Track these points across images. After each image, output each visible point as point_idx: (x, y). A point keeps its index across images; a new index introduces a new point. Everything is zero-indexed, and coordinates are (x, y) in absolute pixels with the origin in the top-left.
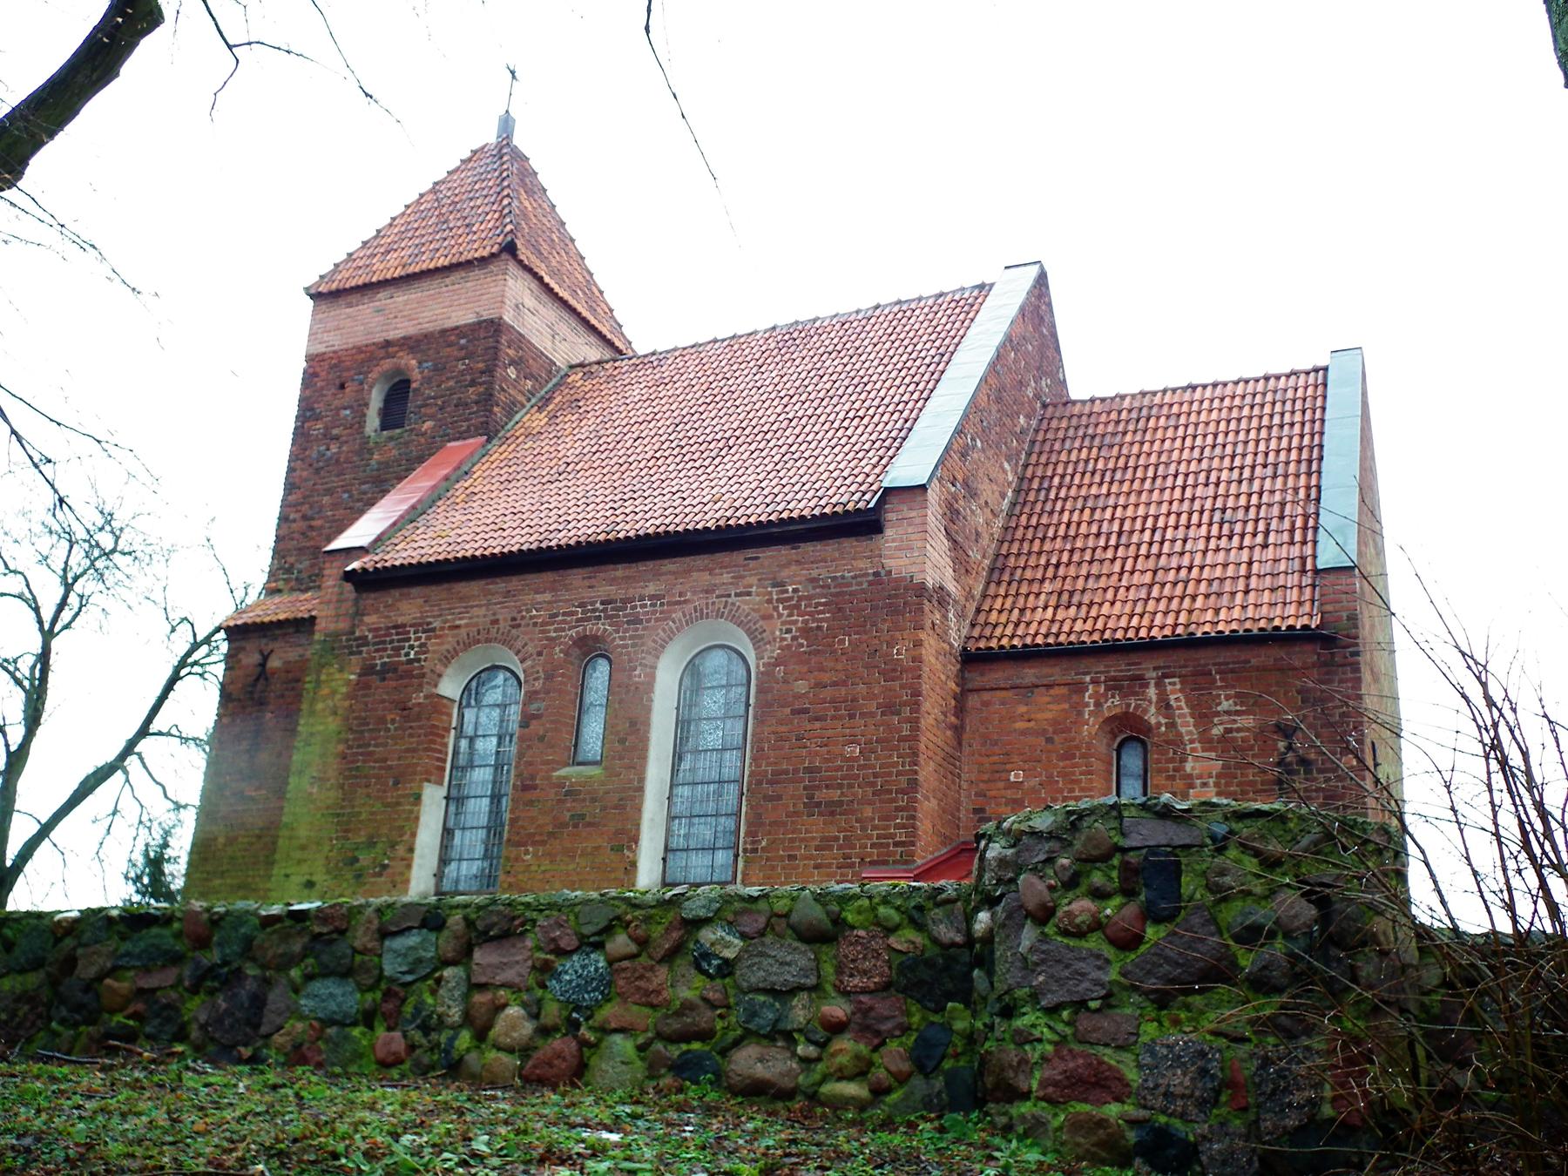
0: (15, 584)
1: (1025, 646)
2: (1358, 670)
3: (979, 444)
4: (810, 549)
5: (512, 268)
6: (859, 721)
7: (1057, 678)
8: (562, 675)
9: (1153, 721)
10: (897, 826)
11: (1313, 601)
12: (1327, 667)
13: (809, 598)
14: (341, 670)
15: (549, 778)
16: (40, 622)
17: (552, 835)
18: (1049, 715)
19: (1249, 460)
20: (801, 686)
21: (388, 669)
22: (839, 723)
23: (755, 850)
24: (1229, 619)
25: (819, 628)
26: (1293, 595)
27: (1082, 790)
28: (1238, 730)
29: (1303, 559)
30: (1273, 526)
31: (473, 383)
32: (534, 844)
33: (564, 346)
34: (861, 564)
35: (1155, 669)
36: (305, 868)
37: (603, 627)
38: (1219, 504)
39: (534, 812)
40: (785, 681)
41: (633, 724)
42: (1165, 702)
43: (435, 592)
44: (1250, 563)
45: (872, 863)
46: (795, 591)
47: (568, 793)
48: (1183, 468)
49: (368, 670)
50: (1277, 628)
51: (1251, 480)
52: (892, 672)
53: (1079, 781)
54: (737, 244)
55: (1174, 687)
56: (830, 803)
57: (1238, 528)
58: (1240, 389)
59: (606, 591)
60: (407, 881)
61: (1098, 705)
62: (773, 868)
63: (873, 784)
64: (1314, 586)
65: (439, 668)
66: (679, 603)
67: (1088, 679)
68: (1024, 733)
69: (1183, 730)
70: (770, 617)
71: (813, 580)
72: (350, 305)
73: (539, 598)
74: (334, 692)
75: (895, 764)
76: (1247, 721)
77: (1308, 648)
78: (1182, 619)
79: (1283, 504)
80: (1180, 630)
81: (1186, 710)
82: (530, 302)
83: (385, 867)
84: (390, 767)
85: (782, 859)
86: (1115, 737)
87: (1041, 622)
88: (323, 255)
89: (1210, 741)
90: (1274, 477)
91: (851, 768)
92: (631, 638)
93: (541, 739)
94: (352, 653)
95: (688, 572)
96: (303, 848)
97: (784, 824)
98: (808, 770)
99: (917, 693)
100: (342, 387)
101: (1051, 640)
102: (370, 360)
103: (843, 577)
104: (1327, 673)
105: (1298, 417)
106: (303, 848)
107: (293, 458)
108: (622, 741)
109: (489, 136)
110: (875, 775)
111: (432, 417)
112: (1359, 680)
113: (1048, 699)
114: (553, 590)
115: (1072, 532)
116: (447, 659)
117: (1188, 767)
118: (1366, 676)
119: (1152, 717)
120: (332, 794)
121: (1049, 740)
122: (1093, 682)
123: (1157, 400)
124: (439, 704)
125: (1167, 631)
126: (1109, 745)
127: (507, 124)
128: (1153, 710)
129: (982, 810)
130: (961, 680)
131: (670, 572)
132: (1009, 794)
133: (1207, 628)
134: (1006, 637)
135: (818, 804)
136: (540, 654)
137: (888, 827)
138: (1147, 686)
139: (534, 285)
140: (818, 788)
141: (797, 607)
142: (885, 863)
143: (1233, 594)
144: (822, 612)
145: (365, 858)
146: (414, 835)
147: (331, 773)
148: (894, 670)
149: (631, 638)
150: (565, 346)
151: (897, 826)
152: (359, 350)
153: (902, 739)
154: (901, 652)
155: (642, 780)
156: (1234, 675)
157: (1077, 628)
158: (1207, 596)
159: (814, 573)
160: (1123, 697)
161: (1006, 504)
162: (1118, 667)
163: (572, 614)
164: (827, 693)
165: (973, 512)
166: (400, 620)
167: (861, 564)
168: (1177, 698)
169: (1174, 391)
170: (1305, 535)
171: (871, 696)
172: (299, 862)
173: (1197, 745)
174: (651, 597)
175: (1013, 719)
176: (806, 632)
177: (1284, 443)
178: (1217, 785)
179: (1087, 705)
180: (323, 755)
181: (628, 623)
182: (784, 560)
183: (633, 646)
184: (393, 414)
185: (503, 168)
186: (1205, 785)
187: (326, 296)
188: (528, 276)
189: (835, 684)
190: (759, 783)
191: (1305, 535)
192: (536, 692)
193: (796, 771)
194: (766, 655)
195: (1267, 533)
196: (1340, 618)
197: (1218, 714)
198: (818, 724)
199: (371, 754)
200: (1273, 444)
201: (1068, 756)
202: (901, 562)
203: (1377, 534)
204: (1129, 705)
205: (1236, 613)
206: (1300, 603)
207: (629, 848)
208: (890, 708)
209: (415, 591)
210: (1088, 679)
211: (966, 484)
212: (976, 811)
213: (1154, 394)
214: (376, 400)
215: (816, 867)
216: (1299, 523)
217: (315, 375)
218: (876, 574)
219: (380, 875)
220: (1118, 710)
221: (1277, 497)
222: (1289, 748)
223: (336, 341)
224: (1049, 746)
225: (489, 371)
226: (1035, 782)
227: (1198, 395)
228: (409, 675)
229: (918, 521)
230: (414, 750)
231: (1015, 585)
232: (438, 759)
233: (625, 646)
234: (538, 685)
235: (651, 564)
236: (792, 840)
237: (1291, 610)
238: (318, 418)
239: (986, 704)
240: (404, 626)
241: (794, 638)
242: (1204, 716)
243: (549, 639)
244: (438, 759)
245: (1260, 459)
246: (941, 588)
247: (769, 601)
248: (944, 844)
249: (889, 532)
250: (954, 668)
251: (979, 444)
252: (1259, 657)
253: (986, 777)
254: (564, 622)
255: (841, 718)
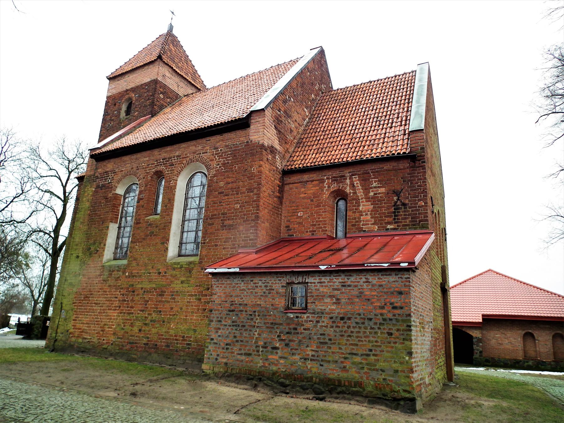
0: (53, 173)
1: (304, 167)
2: (425, 169)
3: (292, 100)
4: (227, 136)
5: (161, 64)
6: (240, 195)
7: (315, 178)
8: (150, 185)
9: (348, 192)
10: (251, 233)
11: (408, 144)
12: (413, 168)
13: (225, 152)
14: (91, 187)
15: (144, 220)
16: (62, 184)
17: (144, 239)
18: (312, 191)
19: (388, 101)
20: (222, 184)
21: (103, 186)
22: (233, 197)
23: (204, 243)
24: (376, 153)
25: (228, 163)
26: (400, 143)
27: (323, 218)
28: (379, 193)
29: (405, 130)
30: (395, 120)
31: (149, 99)
32: (139, 242)
33: (182, 90)
34: (242, 139)
35: (349, 173)
36: (77, 252)
37: (162, 168)
38: (376, 115)
39: (139, 231)
40: (217, 182)
41: (169, 200)
42: (352, 184)
43: (117, 160)
44: (385, 134)
45: (242, 247)
46: (221, 150)
47: (150, 225)
48: (365, 106)
49: (98, 187)
50: (394, 154)
51: (388, 107)
52: (251, 177)
53: (322, 215)
54: (236, 58)
55: (356, 179)
56: (230, 225)
57: (382, 122)
58: (386, 81)
59: (164, 155)
60: (103, 255)
61: (329, 187)
62: (210, 249)
63: (243, 218)
64: (408, 139)
65: (116, 184)
66: (185, 157)
67: (325, 178)
68: (304, 198)
69: (359, 194)
70: (213, 160)
71: (226, 146)
72: (118, 80)
73: (145, 159)
74: (88, 194)
75: (251, 211)
76: (383, 190)
77: (405, 161)
78: (359, 154)
79: (398, 113)
80: (358, 158)
81: (360, 187)
82: (168, 74)
83: (97, 251)
84: (101, 218)
85: (213, 246)
86: (336, 198)
87: (312, 158)
88: (112, 68)
89: (369, 198)
90: (396, 105)
91: (236, 213)
92: (171, 171)
93: (143, 206)
94: (94, 182)
95: (188, 147)
96: (77, 245)
97: (214, 233)
98: (223, 214)
99: (259, 184)
100: (115, 105)
101: (312, 164)
102: (122, 96)
103: (236, 144)
104: (412, 170)
105: (406, 86)
106: (77, 245)
107: (102, 127)
108: (166, 206)
109: (165, 31)
110: (244, 215)
111: (137, 111)
112: (425, 172)
113: (311, 186)
114: (149, 156)
115: (325, 129)
116: (118, 182)
117: (361, 208)
118: (429, 172)
119: (348, 190)
120: (86, 227)
121: (312, 201)
122: (327, 179)
123: (359, 87)
124: (117, 196)
125: (353, 158)
126: (333, 202)
127: (171, 28)
128: (348, 188)
129: (288, 227)
130: (282, 180)
131: (183, 147)
132: (298, 220)
133: (368, 156)
134: (298, 164)
135: (225, 226)
136: (144, 178)
137: (248, 234)
138: (346, 179)
139: (170, 70)
140: (225, 220)
141: (222, 156)
142: (246, 247)
143: (378, 144)
144: (229, 157)
145: (93, 248)
146: (106, 240)
147: (86, 220)
148: (252, 176)
149: (171, 171)
150: (181, 89)
151: (251, 233)
152: (120, 93)
153: (254, 201)
154: (254, 170)
155: (171, 219)
156: (377, 173)
157: (323, 159)
158: (369, 146)
159: (227, 144)
160: (337, 184)
161: (305, 122)
162: (336, 173)
163: (154, 164)
164: (230, 186)
165: (289, 122)
166: (107, 170)
167: (242, 139)
168: (357, 183)
169: (364, 84)
170: (406, 122)
171: (244, 186)
172: (76, 249)
173: (364, 200)
174: (177, 156)
175: (300, 194)
176: (224, 164)
177: (400, 94)
178: (371, 214)
179: (325, 187)
180: (84, 215)
181: (170, 166)
182: (218, 140)
183: (171, 173)
184: (128, 112)
185: (169, 39)
186: (366, 214)
187: (112, 79)
188: (167, 66)
189: (232, 182)
190: (207, 219)
191: (406, 122)
192: (142, 191)
193: (219, 214)
194: (211, 173)
195: (392, 123)
196: (418, 149)
197: (372, 188)
198: (226, 197)
199: (96, 214)
200: (396, 95)
201: (318, 206)
202: (255, 137)
203: (434, 118)
204: (340, 186)
205: (378, 151)
206: (403, 145)
207: (166, 243)
208: (250, 190)
209: (112, 160)
210: (325, 178)
211: (285, 112)
212: (286, 227)
213: (358, 85)
214: (124, 108)
215: (224, 249)
216: (404, 119)
217: (109, 102)
218: (247, 142)
219: (96, 253)
220: (336, 188)
221: (397, 111)
222: (398, 199)
223: (115, 92)
224: (312, 203)
225: (153, 95)
226: (306, 216)
227: (372, 84)
228: (108, 187)
229: (261, 122)
230: (108, 212)
231: (304, 147)
232: (116, 215)
233: (168, 174)
234: (143, 188)
235: (177, 145)
236: (216, 239)
237: (399, 147)
238: (108, 115)
239: (291, 189)
240: (108, 172)
241: (220, 167)
242: (366, 190)
243: (147, 173)
244: (116, 215)
245: (391, 100)
246: (272, 147)
247: (213, 155)
248: (273, 239)
249: (252, 127)
250: (279, 176)
251: (292, 100)
252: (387, 166)
253: (290, 214)
254: (151, 167)
255: (234, 194)
